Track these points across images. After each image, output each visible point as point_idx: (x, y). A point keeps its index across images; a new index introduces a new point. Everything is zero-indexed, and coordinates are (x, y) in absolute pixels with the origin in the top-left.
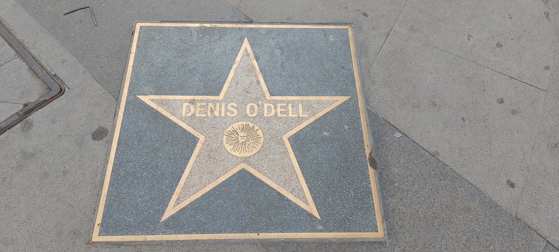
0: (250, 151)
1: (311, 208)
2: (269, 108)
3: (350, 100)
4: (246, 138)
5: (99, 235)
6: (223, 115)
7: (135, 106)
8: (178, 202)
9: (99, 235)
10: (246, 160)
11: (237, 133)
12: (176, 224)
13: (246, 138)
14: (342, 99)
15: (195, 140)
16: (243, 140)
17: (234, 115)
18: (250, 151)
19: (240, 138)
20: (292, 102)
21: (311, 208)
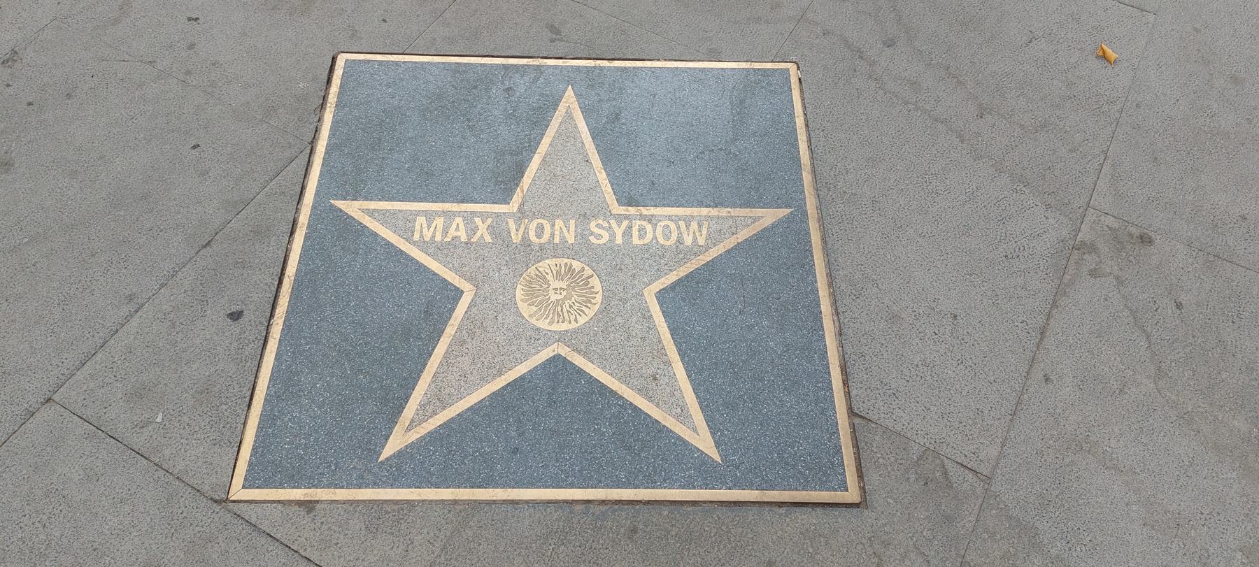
0: (572, 318)
1: (704, 442)
2: (641, 229)
3: (787, 220)
4: (564, 293)
5: (244, 487)
6: (557, 240)
7: (323, 212)
8: (684, 417)
9: (244, 487)
10: (562, 337)
11: (547, 282)
12: (406, 468)
13: (564, 293)
14: (768, 216)
15: (459, 293)
16: (559, 297)
17: (602, 242)
18: (572, 318)
19: (551, 293)
20: (426, 213)
21: (704, 442)
